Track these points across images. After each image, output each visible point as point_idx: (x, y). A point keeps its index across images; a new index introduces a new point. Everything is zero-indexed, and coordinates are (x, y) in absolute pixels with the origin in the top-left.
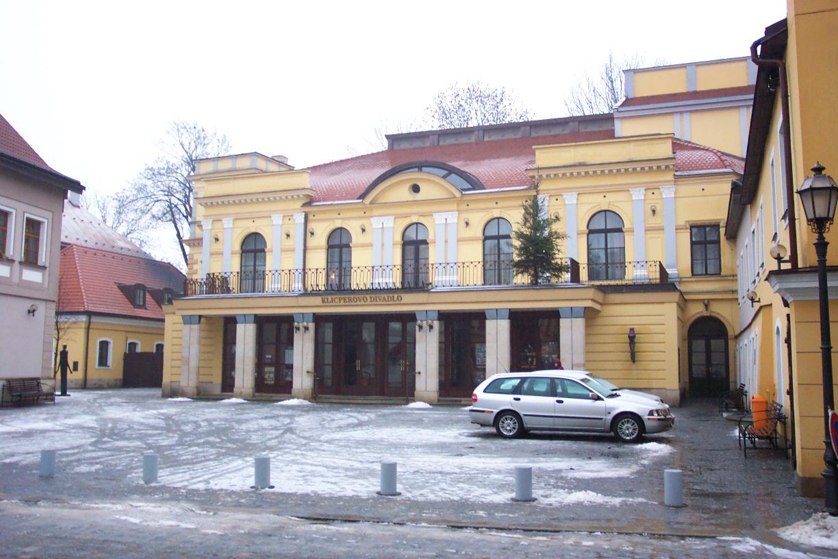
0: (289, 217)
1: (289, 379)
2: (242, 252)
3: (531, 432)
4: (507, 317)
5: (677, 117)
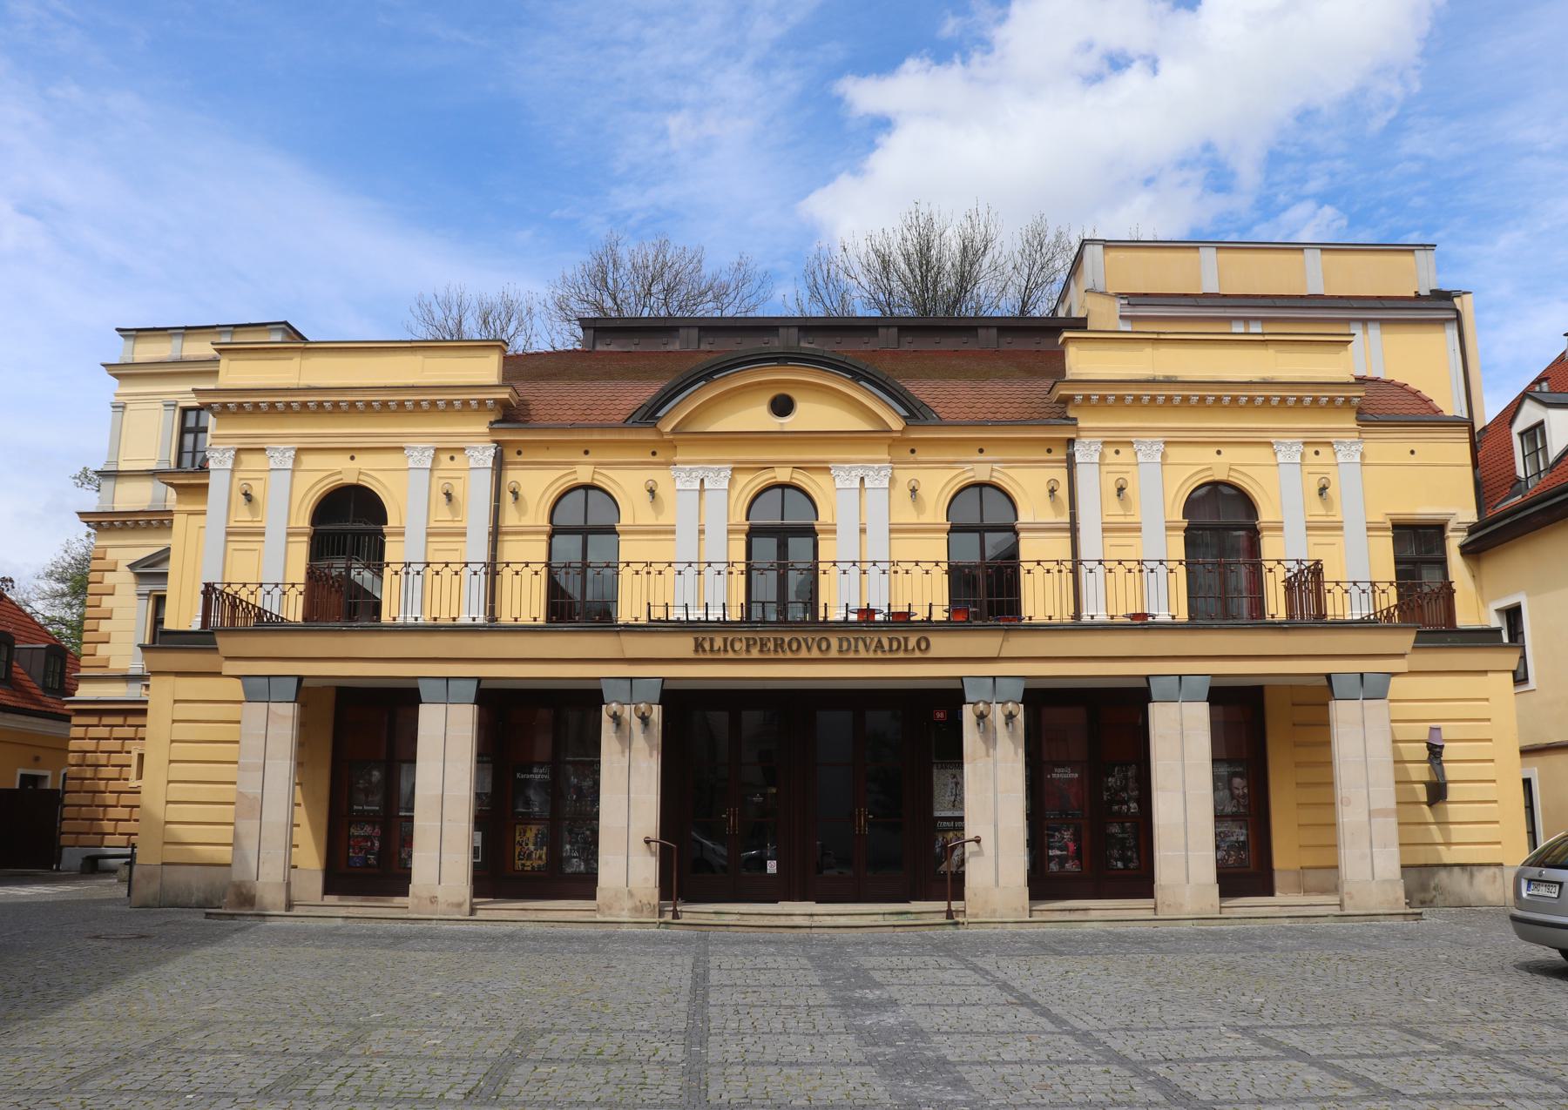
1: (409, 866)
4: (1205, 695)
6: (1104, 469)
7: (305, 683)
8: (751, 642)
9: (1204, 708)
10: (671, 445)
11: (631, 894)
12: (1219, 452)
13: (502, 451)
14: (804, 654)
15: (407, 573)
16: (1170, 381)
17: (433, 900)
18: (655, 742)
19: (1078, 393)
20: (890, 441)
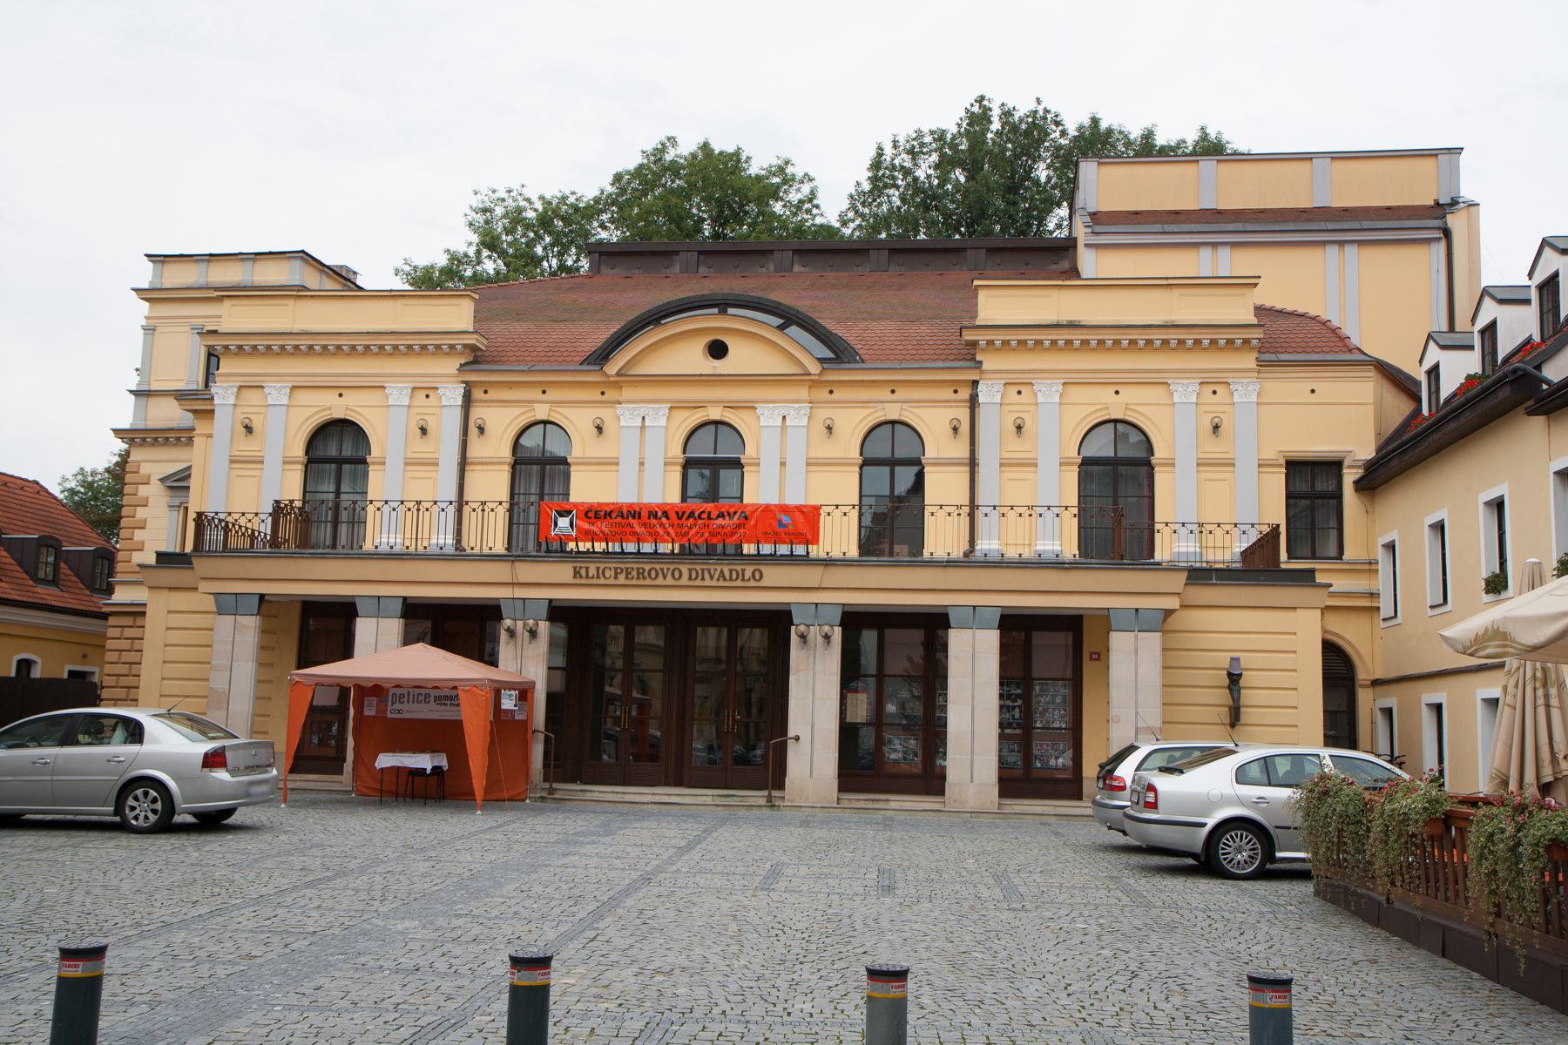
2: (309, 462)
3: (27, 816)
5: (1332, 251)
6: (1006, 408)
7: (266, 598)
8: (619, 571)
10: (617, 385)
13: (470, 391)
14: (660, 581)
15: (483, 510)
16: (1072, 326)
18: (542, 651)
19: (982, 337)
20: (810, 383)
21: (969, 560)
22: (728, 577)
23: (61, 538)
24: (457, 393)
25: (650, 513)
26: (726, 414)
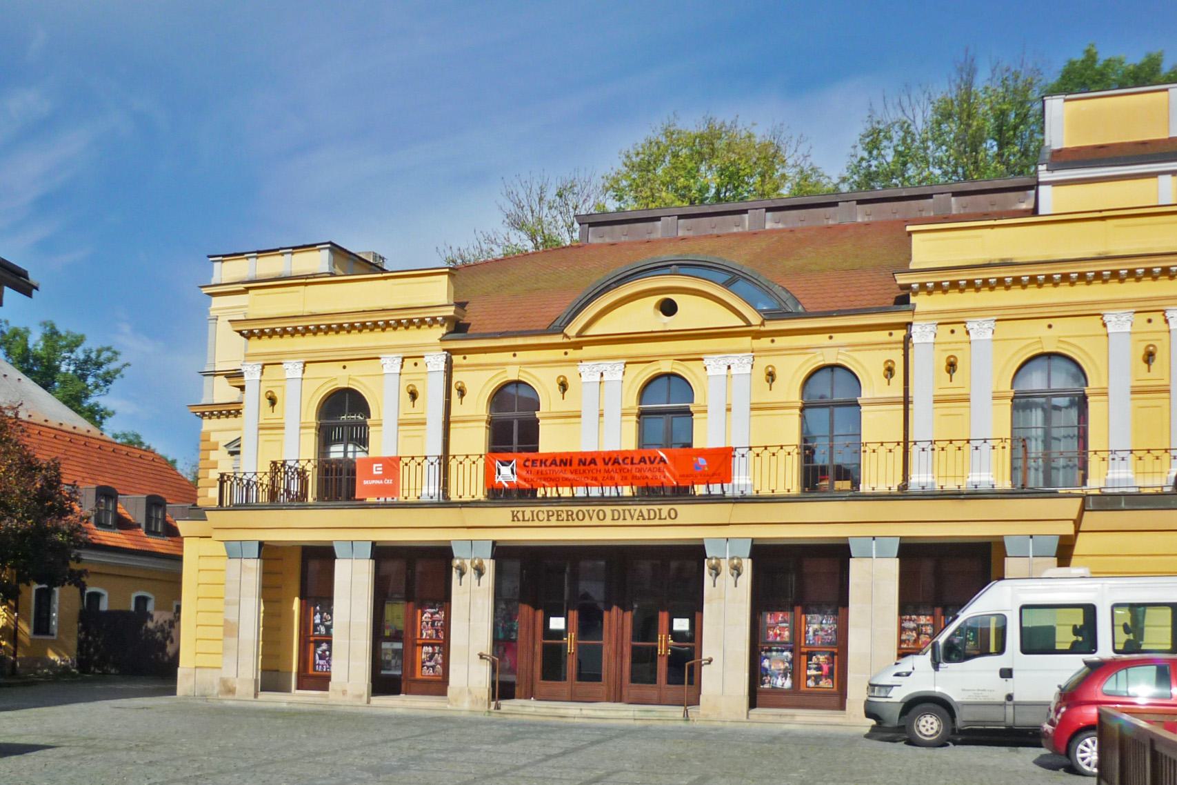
0: (412, 357)
7: (497, 545)
9: (893, 565)
10: (577, 346)
11: (470, 692)
12: (344, 367)
14: (587, 522)
17: (344, 692)
21: (904, 493)
22: (646, 517)
23: (164, 496)
24: (439, 360)
25: (580, 461)
26: (675, 366)
